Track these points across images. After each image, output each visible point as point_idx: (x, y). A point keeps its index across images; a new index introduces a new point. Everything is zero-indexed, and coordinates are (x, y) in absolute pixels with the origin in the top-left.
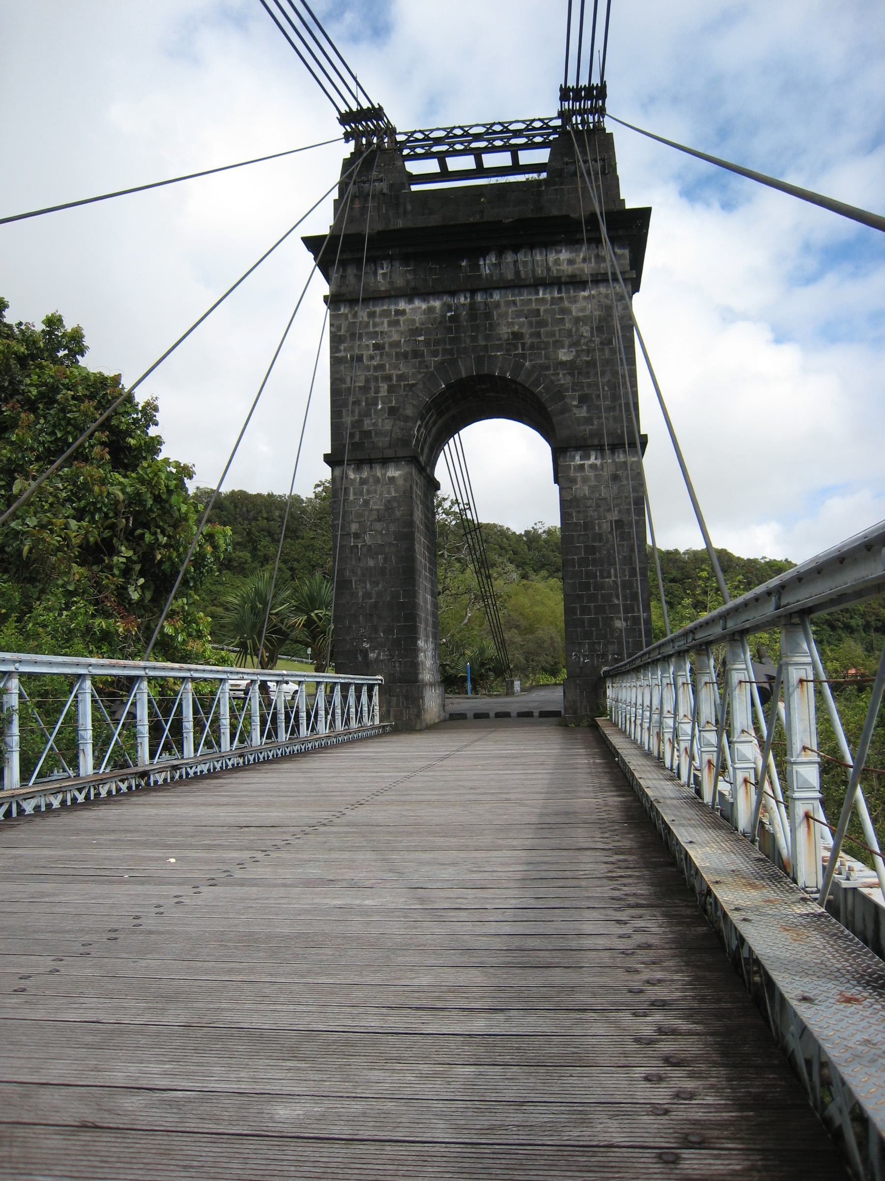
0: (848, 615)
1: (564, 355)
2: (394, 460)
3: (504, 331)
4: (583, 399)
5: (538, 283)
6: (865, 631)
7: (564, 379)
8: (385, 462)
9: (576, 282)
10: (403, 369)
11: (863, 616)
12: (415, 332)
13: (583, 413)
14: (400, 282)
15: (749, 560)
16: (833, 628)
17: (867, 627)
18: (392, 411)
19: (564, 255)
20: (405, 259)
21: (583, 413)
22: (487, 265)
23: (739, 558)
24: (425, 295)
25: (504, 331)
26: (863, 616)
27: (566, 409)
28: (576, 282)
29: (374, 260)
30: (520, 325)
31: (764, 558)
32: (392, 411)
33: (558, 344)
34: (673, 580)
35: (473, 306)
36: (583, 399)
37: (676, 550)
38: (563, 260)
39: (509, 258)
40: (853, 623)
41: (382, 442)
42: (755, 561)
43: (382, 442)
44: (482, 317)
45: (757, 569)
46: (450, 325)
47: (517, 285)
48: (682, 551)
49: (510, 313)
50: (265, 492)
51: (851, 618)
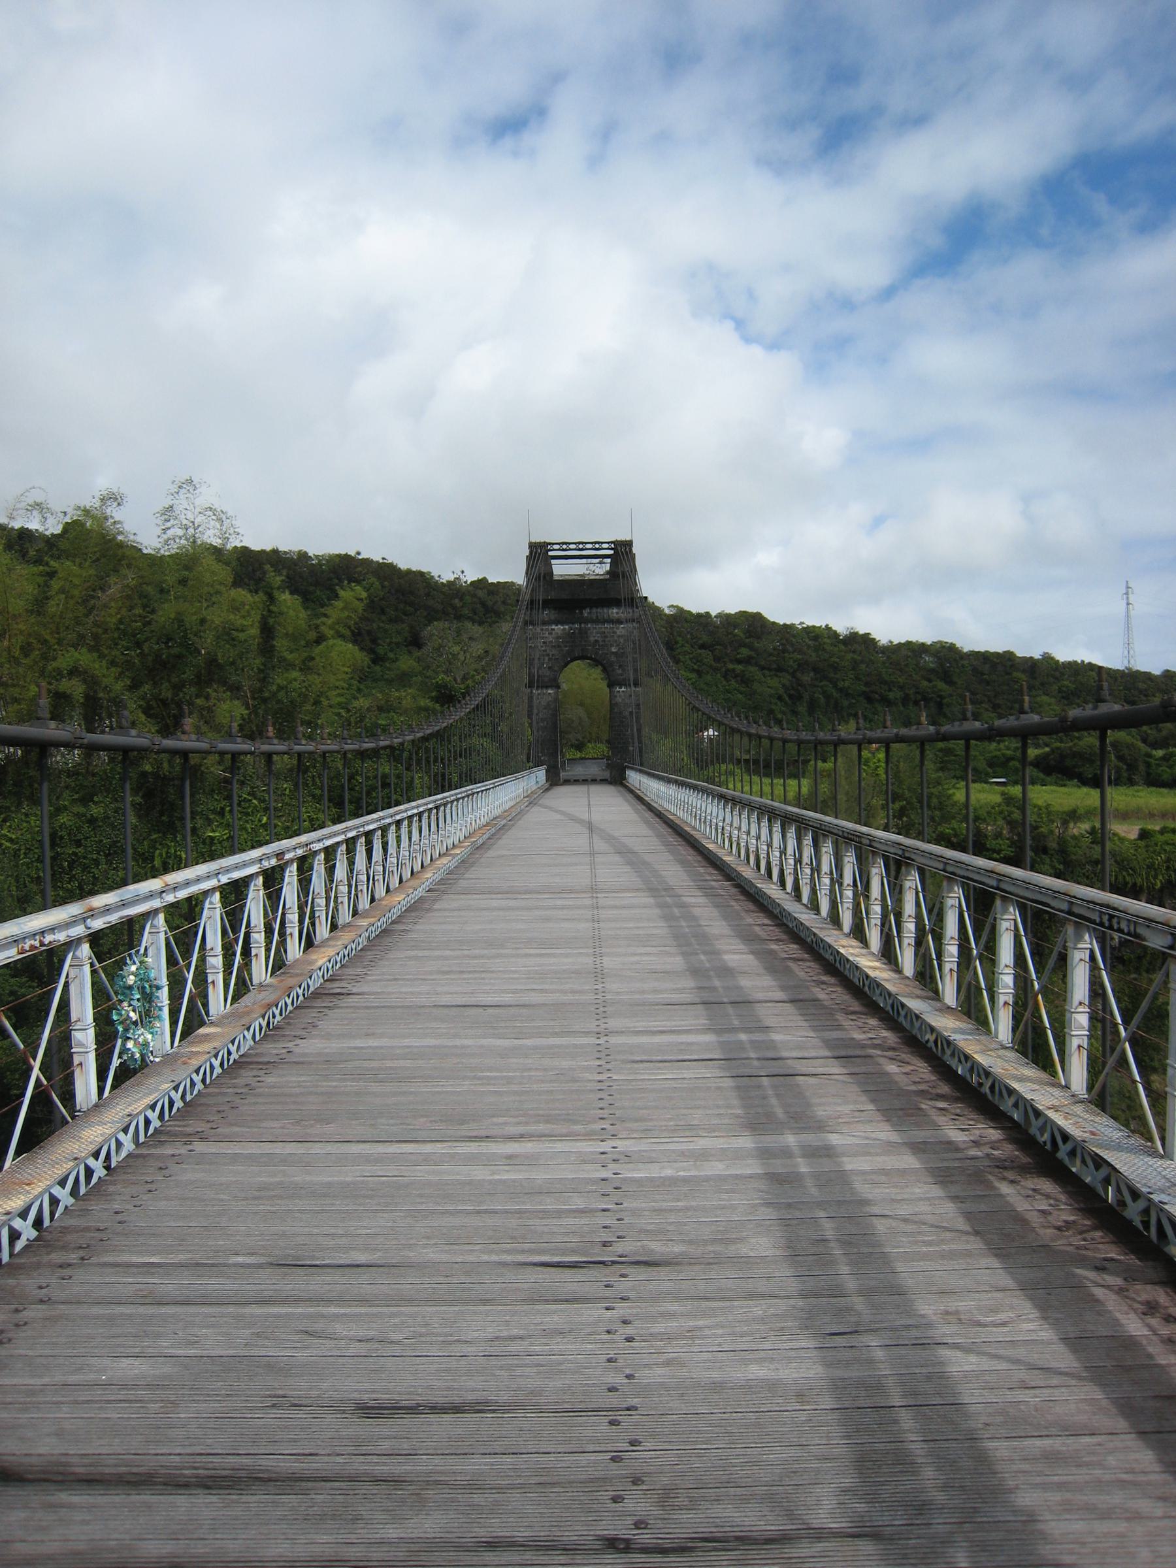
0: (886, 687)
1: (614, 650)
2: (551, 687)
3: (592, 639)
4: (620, 666)
5: (605, 621)
6: (904, 705)
7: (613, 658)
8: (547, 687)
9: (619, 621)
10: (554, 652)
11: (901, 688)
12: (558, 638)
13: (620, 672)
14: (553, 617)
15: (785, 625)
16: (869, 700)
17: (906, 700)
18: (550, 668)
19: (615, 611)
20: (555, 609)
21: (620, 672)
22: (586, 613)
23: (774, 623)
24: (562, 623)
25: (592, 639)
26: (901, 688)
27: (614, 670)
28: (619, 621)
29: (544, 609)
30: (598, 637)
31: (801, 623)
32: (550, 668)
33: (612, 645)
34: (703, 646)
35: (580, 629)
36: (620, 666)
37: (708, 613)
38: (614, 612)
39: (594, 610)
40: (891, 695)
41: (546, 679)
42: (792, 626)
43: (546, 679)
44: (583, 633)
45: (794, 636)
46: (571, 635)
47: (597, 621)
48: (713, 614)
49: (595, 632)
50: (268, 548)
51: (890, 690)
